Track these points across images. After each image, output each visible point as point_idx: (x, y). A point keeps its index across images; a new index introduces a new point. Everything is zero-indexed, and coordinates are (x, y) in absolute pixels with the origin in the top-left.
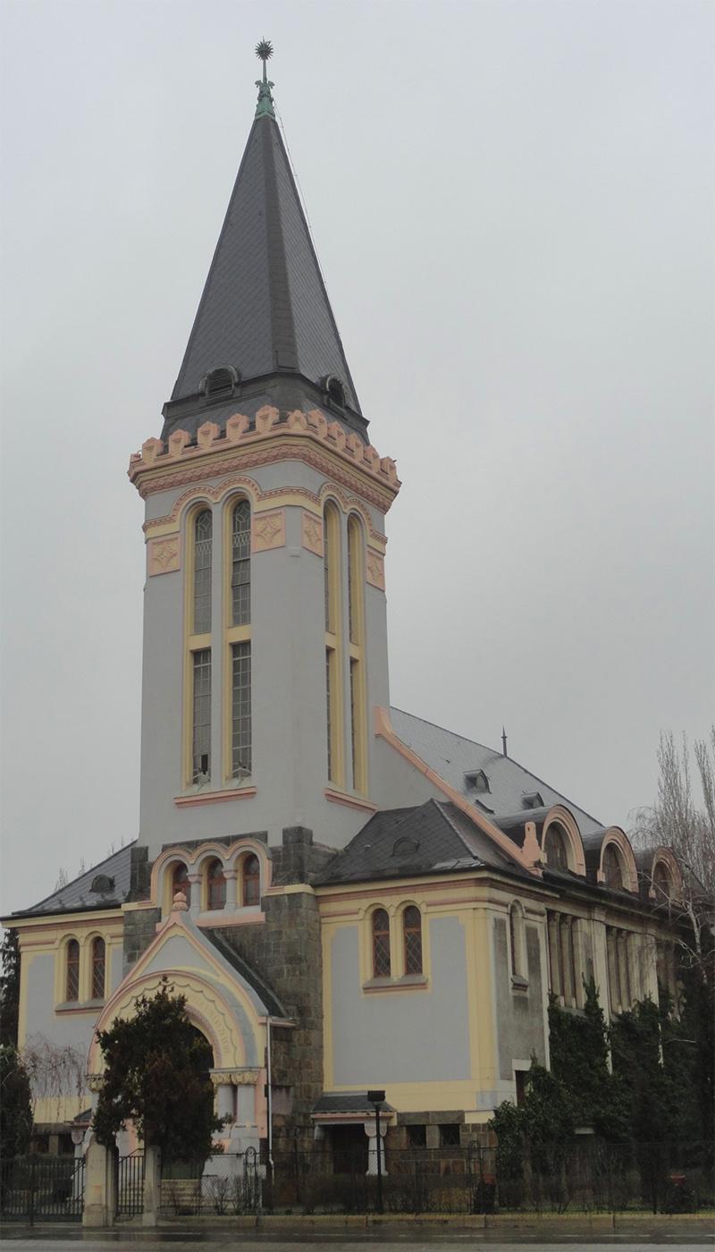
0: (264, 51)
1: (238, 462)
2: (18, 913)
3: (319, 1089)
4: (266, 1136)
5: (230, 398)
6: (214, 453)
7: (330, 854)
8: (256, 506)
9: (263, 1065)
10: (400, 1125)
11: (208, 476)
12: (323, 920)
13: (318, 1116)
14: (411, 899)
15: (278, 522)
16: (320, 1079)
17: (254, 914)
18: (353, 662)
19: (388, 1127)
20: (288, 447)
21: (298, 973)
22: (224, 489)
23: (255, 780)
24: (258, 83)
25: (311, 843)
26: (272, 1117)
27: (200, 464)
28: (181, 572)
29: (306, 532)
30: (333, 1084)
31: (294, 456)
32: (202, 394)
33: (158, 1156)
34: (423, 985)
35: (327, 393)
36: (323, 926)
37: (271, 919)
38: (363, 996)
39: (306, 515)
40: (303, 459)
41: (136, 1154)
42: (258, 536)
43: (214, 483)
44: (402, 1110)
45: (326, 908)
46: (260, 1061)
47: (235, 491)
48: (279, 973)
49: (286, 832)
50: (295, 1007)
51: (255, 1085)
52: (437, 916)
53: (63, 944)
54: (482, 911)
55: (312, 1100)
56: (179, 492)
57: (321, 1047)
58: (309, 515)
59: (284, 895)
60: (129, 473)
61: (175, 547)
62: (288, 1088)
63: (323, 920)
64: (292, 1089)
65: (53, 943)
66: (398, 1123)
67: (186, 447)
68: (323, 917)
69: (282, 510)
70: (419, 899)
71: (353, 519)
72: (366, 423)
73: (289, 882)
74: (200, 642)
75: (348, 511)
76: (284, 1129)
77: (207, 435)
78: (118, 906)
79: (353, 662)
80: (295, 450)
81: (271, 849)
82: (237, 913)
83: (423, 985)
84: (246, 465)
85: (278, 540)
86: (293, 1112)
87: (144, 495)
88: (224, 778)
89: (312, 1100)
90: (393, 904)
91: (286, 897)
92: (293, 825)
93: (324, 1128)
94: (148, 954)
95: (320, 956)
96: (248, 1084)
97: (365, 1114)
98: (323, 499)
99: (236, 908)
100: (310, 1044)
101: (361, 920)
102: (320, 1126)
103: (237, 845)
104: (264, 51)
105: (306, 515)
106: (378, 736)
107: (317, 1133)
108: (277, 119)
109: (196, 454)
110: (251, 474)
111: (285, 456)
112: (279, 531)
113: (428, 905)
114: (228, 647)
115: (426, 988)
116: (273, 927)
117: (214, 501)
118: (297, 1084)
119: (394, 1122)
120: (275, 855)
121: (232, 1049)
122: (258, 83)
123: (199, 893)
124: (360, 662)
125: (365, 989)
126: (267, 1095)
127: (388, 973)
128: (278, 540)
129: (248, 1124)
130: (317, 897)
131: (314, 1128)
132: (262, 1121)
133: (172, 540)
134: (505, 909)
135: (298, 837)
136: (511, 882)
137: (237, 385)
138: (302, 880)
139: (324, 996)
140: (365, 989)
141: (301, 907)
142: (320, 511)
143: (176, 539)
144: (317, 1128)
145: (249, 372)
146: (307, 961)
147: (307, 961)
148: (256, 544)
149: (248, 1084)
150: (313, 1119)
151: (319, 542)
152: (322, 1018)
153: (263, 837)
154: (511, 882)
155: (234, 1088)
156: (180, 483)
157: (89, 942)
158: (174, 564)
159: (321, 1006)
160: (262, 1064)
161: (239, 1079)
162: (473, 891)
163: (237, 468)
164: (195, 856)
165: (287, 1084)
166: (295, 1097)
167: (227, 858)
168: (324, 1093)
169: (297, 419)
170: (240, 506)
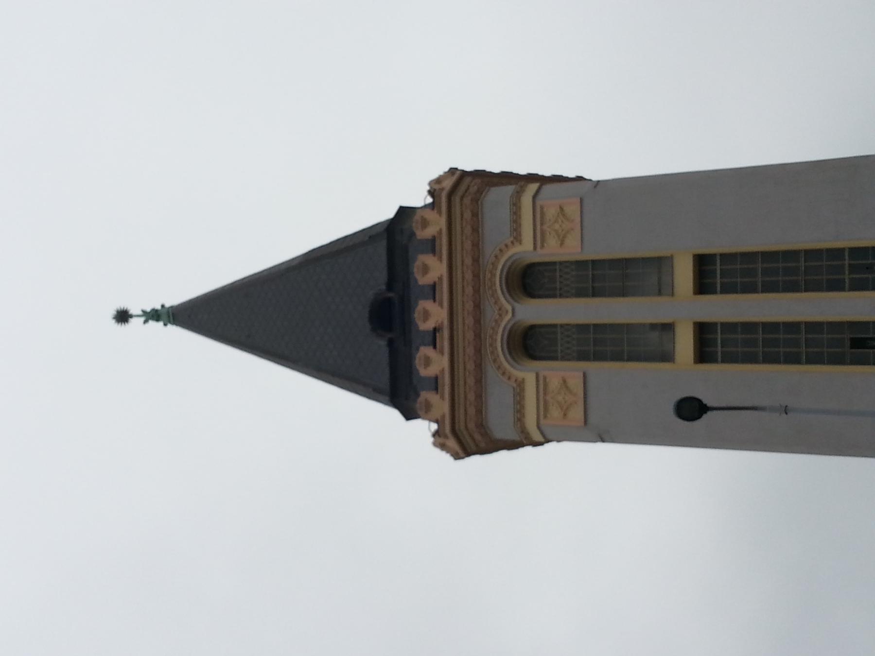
0: (123, 317)
1: (471, 288)
11: (478, 321)
15: (551, 213)
20: (465, 283)
22: (498, 298)
24: (146, 322)
27: (461, 374)
32: (391, 343)
42: (565, 415)
43: (490, 312)
47: (504, 279)
61: (554, 383)
69: (539, 203)
74: (685, 343)
77: (432, 362)
104: (123, 317)
110: (489, 250)
112: (561, 208)
117: (510, 315)
122: (146, 322)
143: (545, 378)
145: (381, 276)
158: (576, 383)
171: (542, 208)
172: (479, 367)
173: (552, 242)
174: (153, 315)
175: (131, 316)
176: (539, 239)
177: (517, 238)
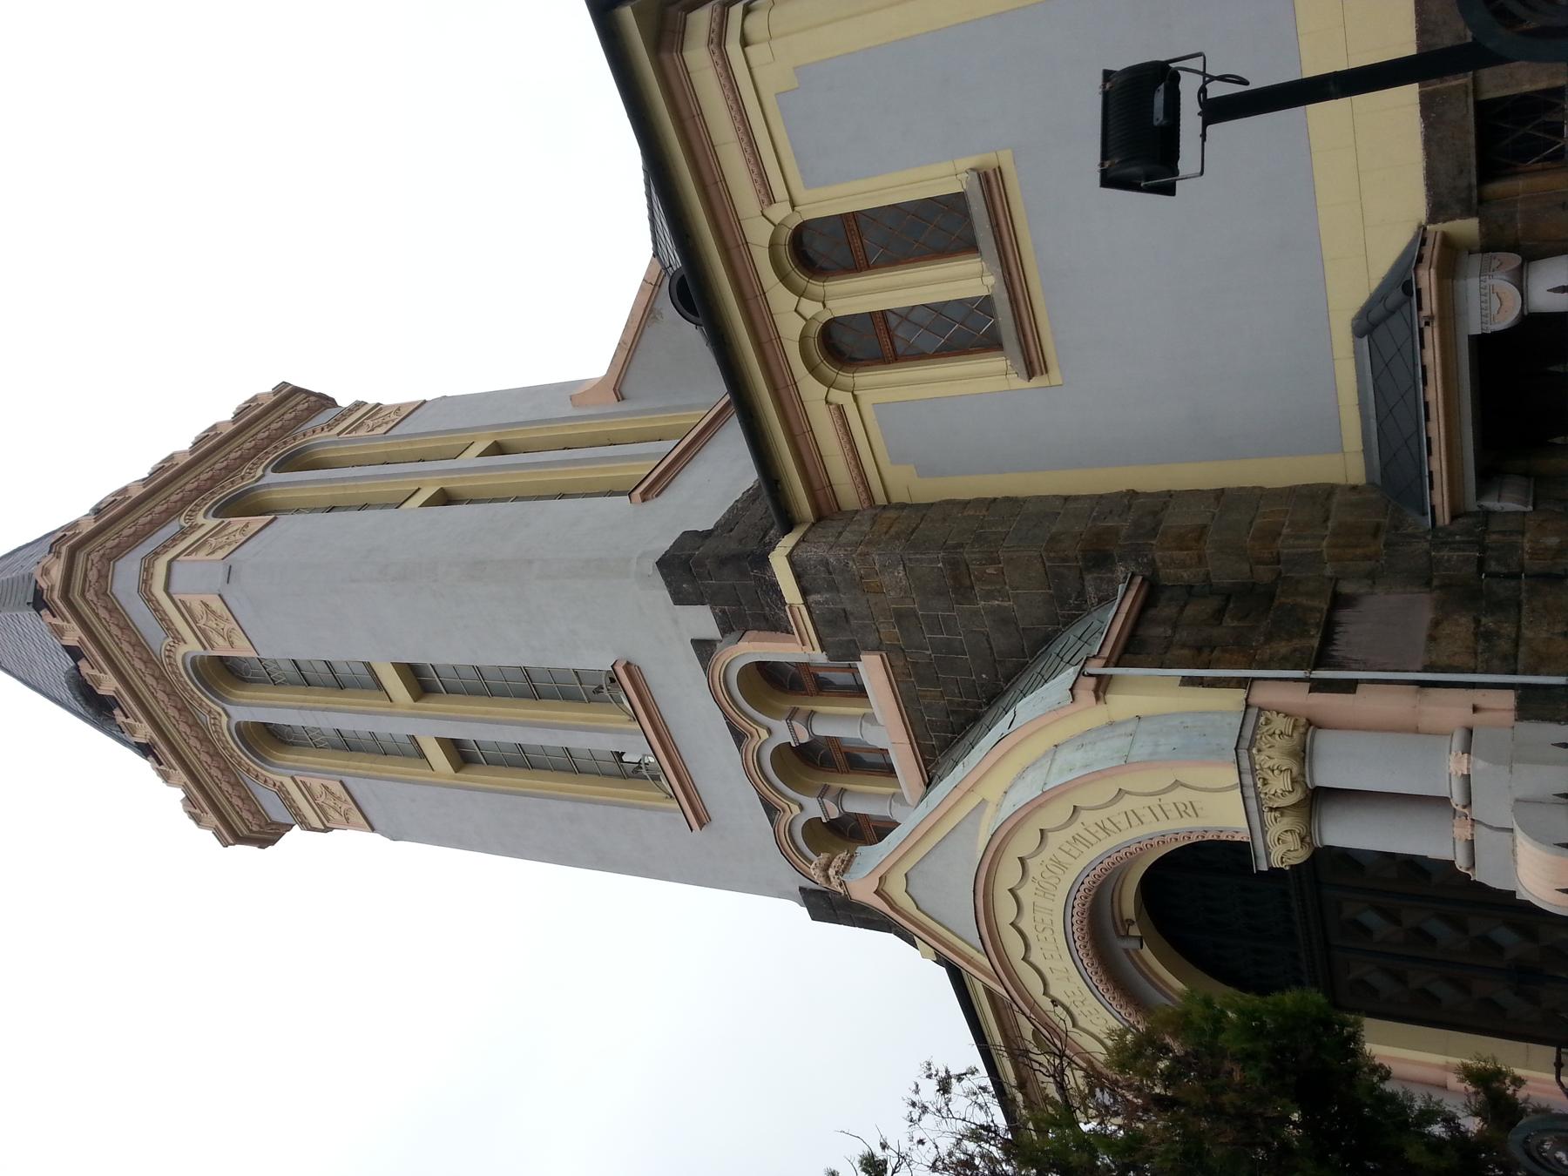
3: (1354, 497)
4: (1508, 699)
9: (1240, 694)
10: (1474, 206)
13: (1440, 497)
14: (766, 252)
16: (1317, 496)
17: (871, 670)
18: (497, 449)
19: (1485, 249)
21: (991, 570)
25: (707, 534)
26: (1437, 669)
30: (1343, 460)
34: (990, 181)
37: (872, 639)
38: (1055, 376)
40: (110, 560)
44: (1417, 207)
45: (846, 491)
48: (1004, 620)
50: (1088, 577)
51: (1310, 723)
54: (750, 19)
55: (1386, 521)
57: (1220, 494)
59: (806, 603)
63: (880, 499)
64: (1346, 588)
66: (1467, 213)
68: (870, 497)
76: (1488, 622)
80: (93, 575)
81: (724, 632)
82: (878, 720)
83: (990, 181)
86: (1428, 583)
89: (1386, 521)
90: (794, 312)
91: (812, 598)
93: (1488, 477)
94: (968, 962)
95: (965, 504)
96: (1302, 755)
97: (1432, 335)
99: (870, 718)
101: (855, 398)
102: (1481, 492)
103: (743, 723)
106: (620, 397)
107: (1507, 502)
113: (771, 199)
114: (418, 704)
115: (999, 171)
116: (890, 632)
118: (1329, 571)
119: (1467, 227)
120: (732, 625)
121: (1180, 795)
123: (863, 799)
124: (498, 439)
125: (1031, 374)
126: (1349, 687)
127: (960, 196)
128: (217, 605)
129: (1457, 764)
130: (820, 517)
131: (1488, 513)
132: (1450, 709)
133: (308, 789)
138: (763, 562)
139: (1073, 492)
140: (1031, 374)
141: (826, 564)
144: (1491, 504)
146: (961, 545)
147: (961, 545)
149: (1302, 755)
150: (1454, 517)
152: (1133, 494)
155: (1317, 799)
159: (1099, 498)
160: (1237, 696)
161: (1279, 783)
162: (698, 57)
164: (782, 803)
166: (1372, 577)
167: (764, 734)
168: (1370, 483)
171: (183, 602)
172: (237, 784)
176: (203, 637)
177: (178, 638)
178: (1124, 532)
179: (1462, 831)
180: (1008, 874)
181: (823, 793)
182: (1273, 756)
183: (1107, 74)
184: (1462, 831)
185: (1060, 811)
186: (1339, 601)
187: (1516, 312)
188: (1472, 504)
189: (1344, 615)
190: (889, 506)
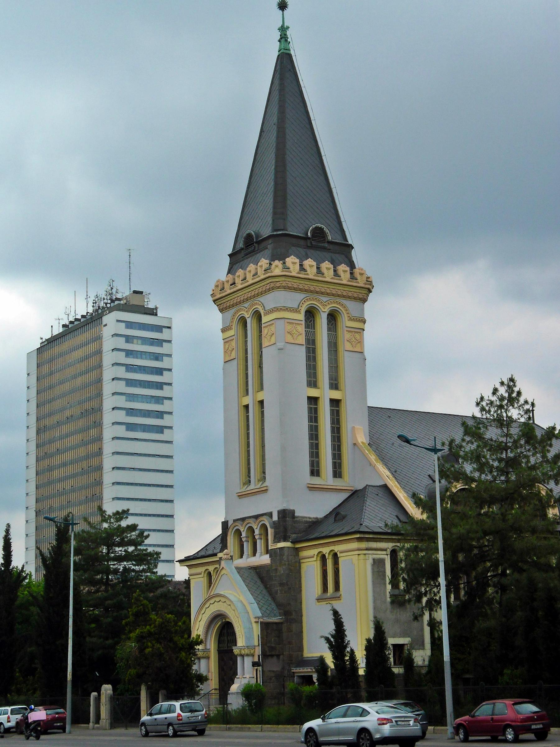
0: (283, 6)
2: (188, 557)
5: (254, 251)
6: (245, 288)
7: (310, 522)
8: (264, 319)
12: (302, 561)
15: (272, 328)
23: (267, 483)
28: (236, 360)
29: (288, 332)
31: (279, 288)
33: (165, 695)
35: (309, 238)
36: (302, 564)
39: (288, 322)
41: (213, 691)
46: (256, 641)
48: (276, 592)
49: (279, 512)
51: (253, 655)
52: (346, 558)
53: (319, 558)
56: (232, 311)
58: (291, 322)
60: (212, 295)
62: (278, 656)
63: (302, 561)
64: (281, 657)
65: (201, 574)
67: (231, 285)
70: (337, 548)
71: (333, 317)
72: (351, 247)
73: (279, 542)
74: (313, 393)
75: (327, 309)
78: (215, 555)
79: (335, 403)
80: (278, 284)
84: (258, 295)
85: (273, 340)
87: (221, 311)
88: (257, 480)
90: (326, 550)
92: (282, 508)
98: (303, 309)
100: (292, 631)
105: (288, 322)
108: (292, 52)
109: (235, 289)
110: (262, 299)
111: (273, 288)
114: (242, 407)
120: (275, 525)
128: (273, 340)
131: (294, 677)
134: (384, 552)
135: (285, 514)
136: (386, 537)
137: (256, 242)
138: (285, 540)
142: (301, 316)
143: (273, 324)
147: (288, 585)
148: (265, 343)
151: (300, 337)
153: (270, 515)
154: (386, 537)
156: (233, 306)
157: (331, 557)
158: (233, 355)
160: (256, 644)
163: (254, 296)
165: (277, 653)
169: (277, 266)
170: (258, 316)
173: (348, 336)
174: (283, 30)
175: (283, 11)
178: (292, 617)
179: (241, 677)
180: (217, 599)
181: (260, 534)
182: (247, 651)
183: (383, 623)
184: (241, 677)
185: (233, 608)
186: (278, 656)
187: (304, 744)
188: (296, 675)
189: (275, 658)
190: (300, 563)
